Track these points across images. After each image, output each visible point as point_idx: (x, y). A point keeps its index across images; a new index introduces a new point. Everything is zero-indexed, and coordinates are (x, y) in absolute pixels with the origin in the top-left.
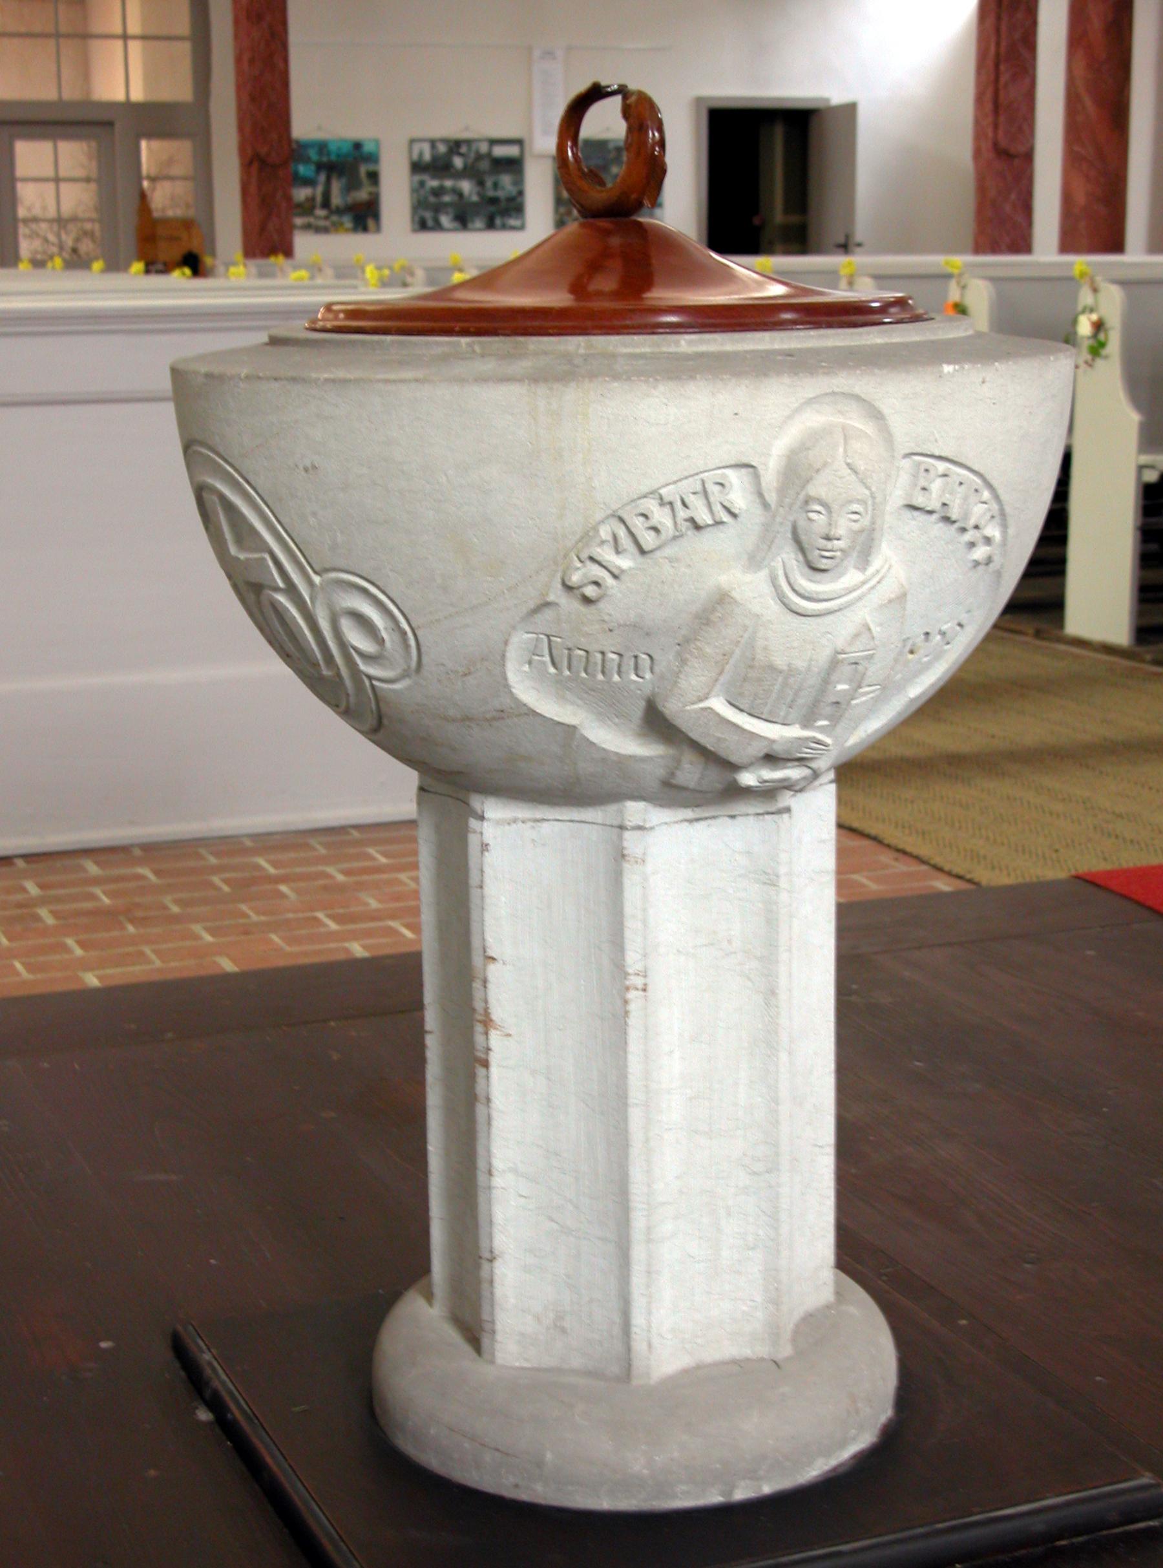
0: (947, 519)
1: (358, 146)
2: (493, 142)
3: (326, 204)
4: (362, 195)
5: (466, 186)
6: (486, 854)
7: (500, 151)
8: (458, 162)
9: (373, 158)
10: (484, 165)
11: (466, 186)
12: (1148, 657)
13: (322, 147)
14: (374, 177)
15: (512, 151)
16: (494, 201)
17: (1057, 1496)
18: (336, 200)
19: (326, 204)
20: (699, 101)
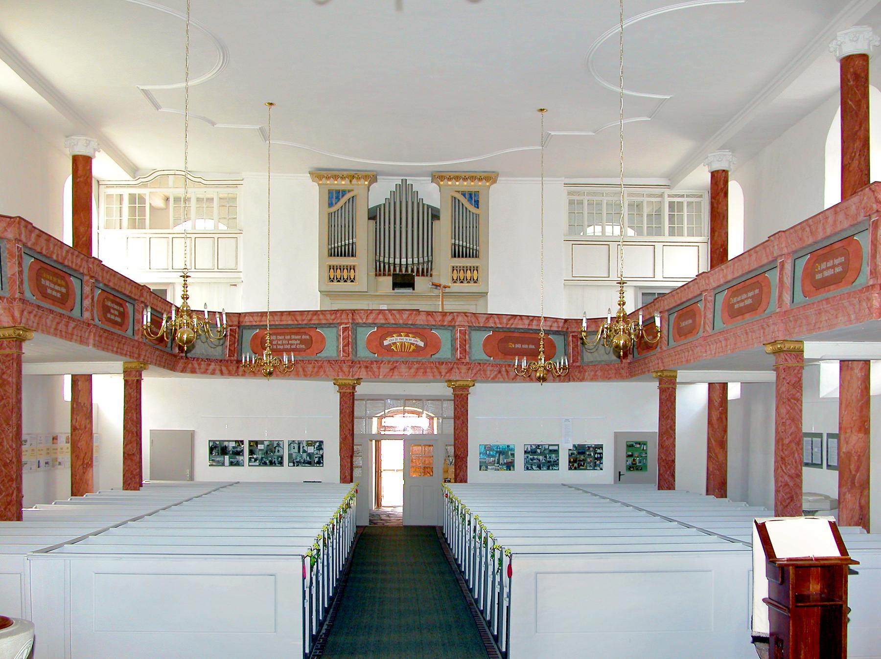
0: (198, 359)
1: (508, 446)
2: (549, 445)
3: (498, 463)
4: (510, 460)
5: (541, 458)
6: (436, 223)
7: (551, 448)
8: (539, 451)
9: (513, 450)
10: (547, 452)
11: (541, 458)
12: (293, 451)
13: (498, 447)
14: (513, 455)
15: (556, 448)
16: (549, 462)
17: (152, 442)
18: (501, 462)
19: (498, 463)
20: (616, 435)
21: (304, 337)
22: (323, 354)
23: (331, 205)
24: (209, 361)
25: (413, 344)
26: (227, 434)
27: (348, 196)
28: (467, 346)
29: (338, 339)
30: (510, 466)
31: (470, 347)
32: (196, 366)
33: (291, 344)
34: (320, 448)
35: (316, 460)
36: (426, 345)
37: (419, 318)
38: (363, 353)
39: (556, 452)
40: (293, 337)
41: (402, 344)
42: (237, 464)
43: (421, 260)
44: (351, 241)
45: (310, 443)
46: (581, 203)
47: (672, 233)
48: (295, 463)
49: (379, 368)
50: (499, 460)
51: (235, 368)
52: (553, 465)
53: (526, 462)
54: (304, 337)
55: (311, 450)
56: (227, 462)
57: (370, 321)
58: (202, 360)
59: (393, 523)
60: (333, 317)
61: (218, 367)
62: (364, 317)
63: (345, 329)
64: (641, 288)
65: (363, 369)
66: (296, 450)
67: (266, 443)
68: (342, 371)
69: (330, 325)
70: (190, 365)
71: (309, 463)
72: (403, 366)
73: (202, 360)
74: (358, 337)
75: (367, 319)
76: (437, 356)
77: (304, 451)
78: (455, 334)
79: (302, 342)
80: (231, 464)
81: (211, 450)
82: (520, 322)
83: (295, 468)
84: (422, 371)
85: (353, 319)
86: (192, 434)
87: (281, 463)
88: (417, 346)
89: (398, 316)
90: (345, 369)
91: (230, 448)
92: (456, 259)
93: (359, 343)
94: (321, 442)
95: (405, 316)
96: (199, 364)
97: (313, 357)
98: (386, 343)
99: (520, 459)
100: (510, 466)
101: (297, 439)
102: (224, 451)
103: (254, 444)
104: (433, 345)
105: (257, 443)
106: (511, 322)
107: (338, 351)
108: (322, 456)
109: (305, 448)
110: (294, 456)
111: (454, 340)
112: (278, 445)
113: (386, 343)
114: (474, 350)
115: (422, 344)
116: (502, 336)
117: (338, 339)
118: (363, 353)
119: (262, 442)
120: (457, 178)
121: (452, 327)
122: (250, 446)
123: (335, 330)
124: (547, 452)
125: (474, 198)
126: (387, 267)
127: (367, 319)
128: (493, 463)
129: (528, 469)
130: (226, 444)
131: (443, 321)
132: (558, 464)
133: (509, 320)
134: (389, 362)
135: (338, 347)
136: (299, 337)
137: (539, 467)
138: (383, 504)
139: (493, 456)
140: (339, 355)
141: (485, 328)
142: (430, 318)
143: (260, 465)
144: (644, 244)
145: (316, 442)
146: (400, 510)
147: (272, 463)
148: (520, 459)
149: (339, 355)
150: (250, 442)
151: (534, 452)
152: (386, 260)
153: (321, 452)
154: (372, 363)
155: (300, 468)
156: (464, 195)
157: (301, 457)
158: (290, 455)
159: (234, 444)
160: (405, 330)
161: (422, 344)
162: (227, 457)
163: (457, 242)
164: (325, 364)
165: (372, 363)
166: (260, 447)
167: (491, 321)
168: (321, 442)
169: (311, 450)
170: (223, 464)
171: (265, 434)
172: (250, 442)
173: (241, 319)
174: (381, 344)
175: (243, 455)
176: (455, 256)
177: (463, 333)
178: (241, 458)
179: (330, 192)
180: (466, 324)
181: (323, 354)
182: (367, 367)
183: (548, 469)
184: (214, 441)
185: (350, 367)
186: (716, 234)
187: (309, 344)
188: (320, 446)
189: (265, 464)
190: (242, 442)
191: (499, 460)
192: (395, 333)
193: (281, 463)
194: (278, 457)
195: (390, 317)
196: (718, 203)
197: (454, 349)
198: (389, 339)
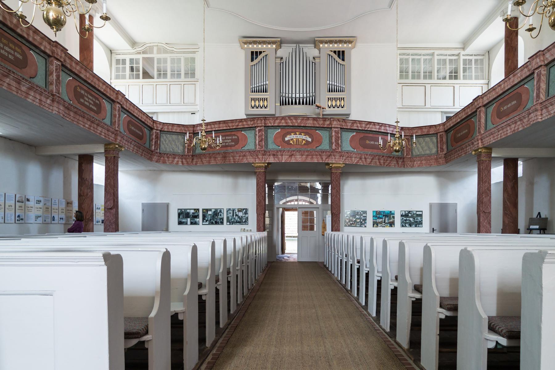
0: (167, 154)
3: (384, 222)
4: (391, 220)
5: (411, 219)
8: (410, 215)
10: (415, 215)
11: (411, 219)
12: (229, 215)
14: (394, 217)
16: (416, 222)
18: (386, 221)
19: (384, 222)
21: (234, 137)
22: (246, 148)
23: (252, 60)
24: (174, 155)
25: (304, 140)
26: (189, 205)
27: (263, 54)
28: (340, 141)
29: (255, 137)
30: (392, 224)
31: (341, 142)
32: (166, 159)
33: (226, 143)
34: (246, 213)
35: (244, 220)
36: (312, 140)
37: (309, 122)
38: (272, 146)
39: (421, 216)
40: (227, 138)
41: (297, 140)
42: (195, 223)
43: (308, 95)
44: (265, 83)
45: (240, 210)
46: (407, 60)
47: (465, 78)
48: (230, 222)
49: (282, 155)
50: (385, 220)
51: (191, 160)
52: (419, 224)
53: (402, 222)
54: (234, 137)
55: (240, 214)
56: (189, 223)
57: (276, 125)
58: (170, 155)
59: (291, 260)
60: (252, 123)
61: (180, 160)
62: (272, 122)
63: (260, 131)
64: (446, 113)
65: (271, 157)
66: (231, 215)
67: (213, 210)
68: (258, 158)
69: (250, 128)
70: (162, 158)
71: (239, 222)
72: (298, 153)
73: (170, 155)
74: (268, 136)
75: (274, 123)
76: (320, 148)
77: (236, 215)
78: (332, 133)
79: (233, 140)
80: (192, 223)
81: (179, 215)
82: (374, 127)
83: (231, 226)
84: (310, 157)
85: (265, 123)
86: (167, 205)
87: (222, 223)
88: (307, 141)
89: (294, 121)
90: (260, 156)
91: (191, 214)
92: (331, 93)
93: (269, 139)
94: (246, 210)
95: (299, 121)
96: (168, 158)
97: (240, 150)
98: (286, 139)
99: (398, 220)
100: (392, 224)
101: (232, 207)
102: (187, 215)
103: (206, 211)
104: (317, 140)
105: (207, 210)
106: (368, 126)
107: (255, 145)
108: (247, 218)
109: (237, 213)
110: (230, 218)
111: (331, 137)
112: (220, 211)
113: (286, 139)
114: (344, 144)
115: (310, 140)
116: (362, 135)
117: (255, 137)
118: (272, 146)
119: (210, 210)
120: (331, 42)
121: (330, 128)
122: (203, 212)
123: (253, 132)
124: (415, 215)
125: (341, 54)
126: (287, 100)
127: (274, 123)
128: (381, 223)
129: (403, 226)
130: (188, 211)
131: (324, 124)
132: (422, 224)
133: (367, 124)
134: (289, 151)
135: (255, 142)
136: (230, 138)
137: (410, 225)
138: (286, 251)
139: (381, 218)
140: (256, 148)
141: (351, 130)
142: (315, 122)
143: (209, 224)
144: (448, 85)
145: (244, 209)
146: (295, 256)
147: (217, 223)
148: (398, 220)
149: (256, 148)
150: (203, 210)
151: (406, 216)
152: (287, 95)
153: (247, 216)
154: (277, 152)
155: (233, 226)
156: (335, 52)
157: (235, 219)
158: (228, 218)
159: (193, 211)
160: (299, 130)
161: (310, 140)
162: (189, 219)
163: (331, 83)
164: (247, 153)
165: (277, 152)
166: (210, 213)
167: (355, 125)
168: (246, 210)
169: (240, 214)
170: (186, 224)
171: (213, 205)
172: (203, 210)
173: (195, 129)
174: (284, 139)
175: (199, 218)
176: (329, 91)
177: (337, 133)
178: (197, 220)
179: (252, 53)
180: (339, 126)
181: (246, 148)
182: (274, 155)
183: (416, 226)
184: (181, 210)
185: (263, 155)
186: (510, 61)
187: (237, 141)
188: (246, 211)
189: (212, 223)
190: (198, 210)
191: (385, 220)
192: (292, 132)
193: (222, 223)
194: (220, 219)
195: (289, 122)
196: (511, 40)
197: (331, 143)
198: (288, 136)
